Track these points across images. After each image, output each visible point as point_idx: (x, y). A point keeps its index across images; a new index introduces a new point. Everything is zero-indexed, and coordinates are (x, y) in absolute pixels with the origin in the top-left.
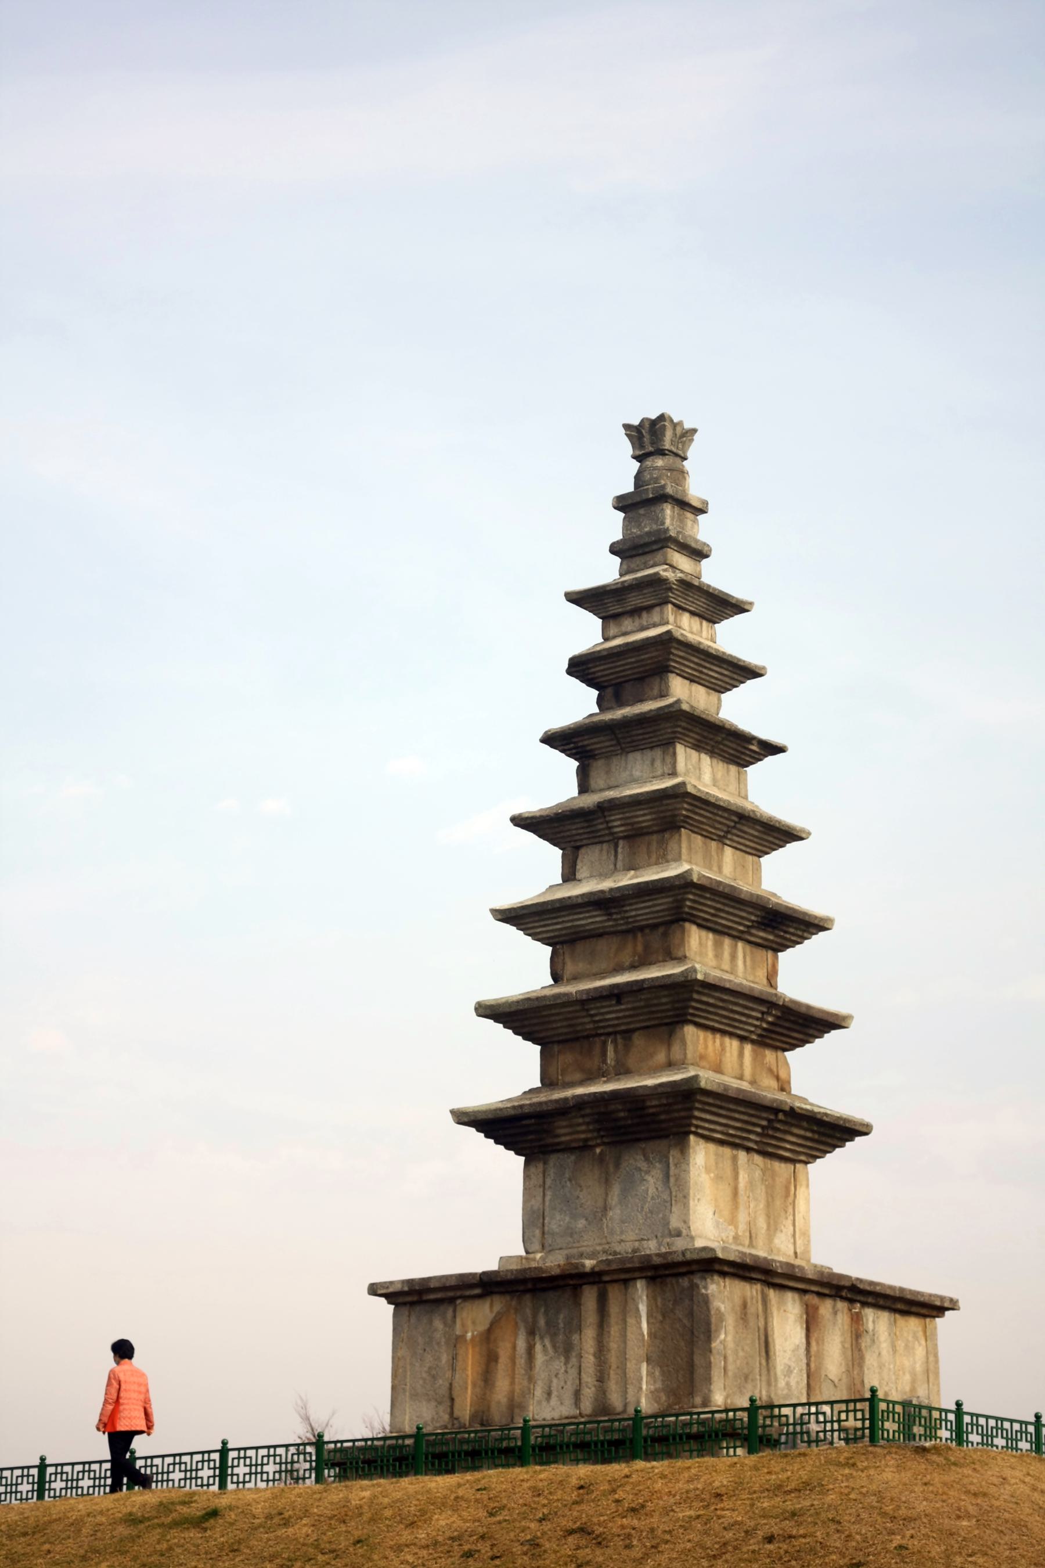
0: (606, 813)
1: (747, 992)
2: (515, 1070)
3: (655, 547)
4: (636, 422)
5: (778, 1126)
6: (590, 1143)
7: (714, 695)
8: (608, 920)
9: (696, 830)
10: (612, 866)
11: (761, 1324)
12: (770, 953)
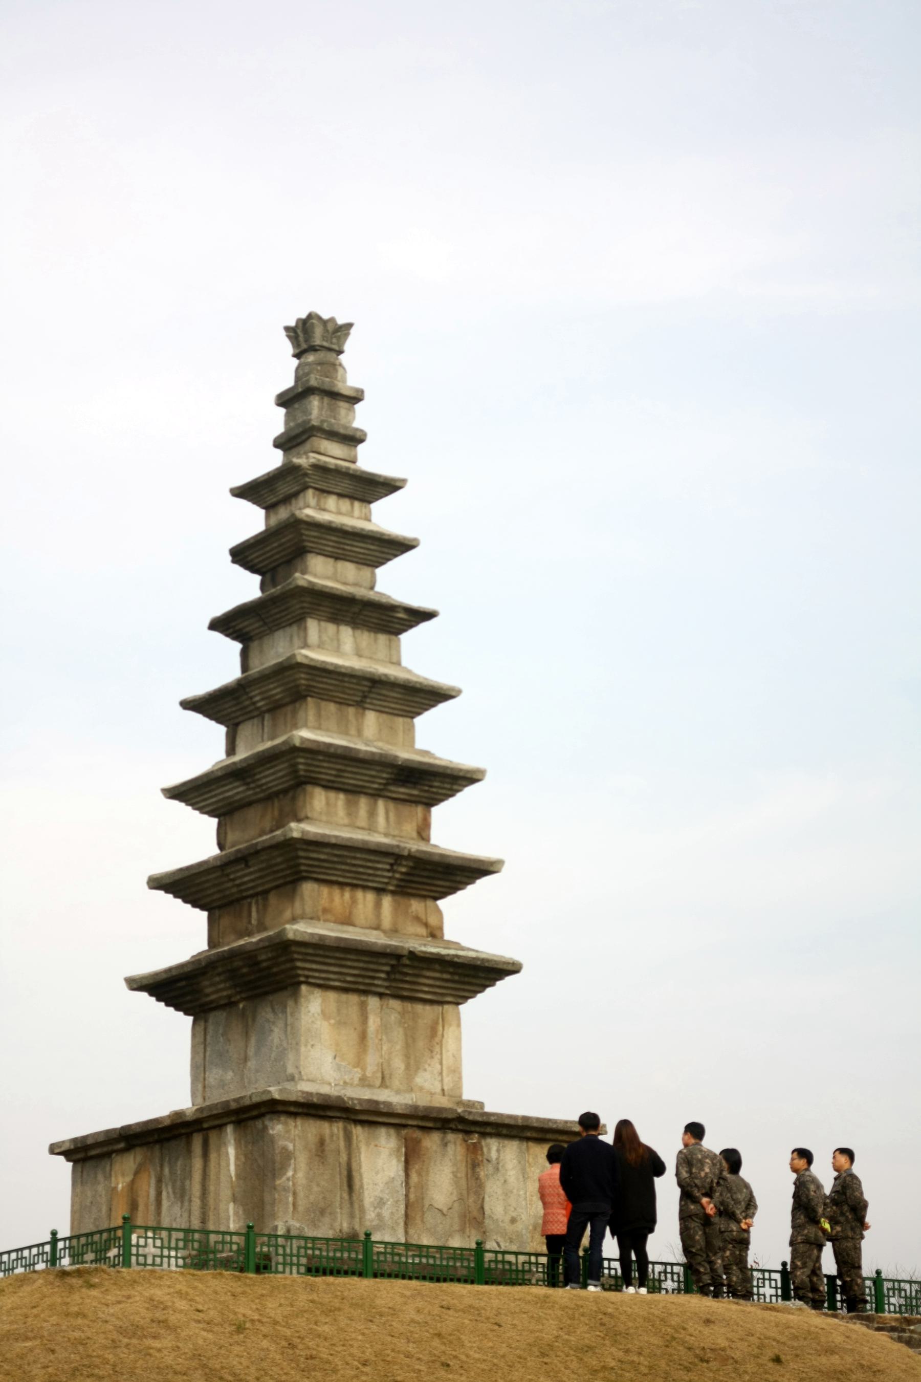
0: (247, 690)
1: (360, 846)
3: (304, 437)
4: (293, 324)
5: (405, 970)
6: (233, 999)
7: (366, 572)
8: (248, 789)
9: (325, 697)
10: (260, 739)
11: (344, 1158)
12: (420, 809)
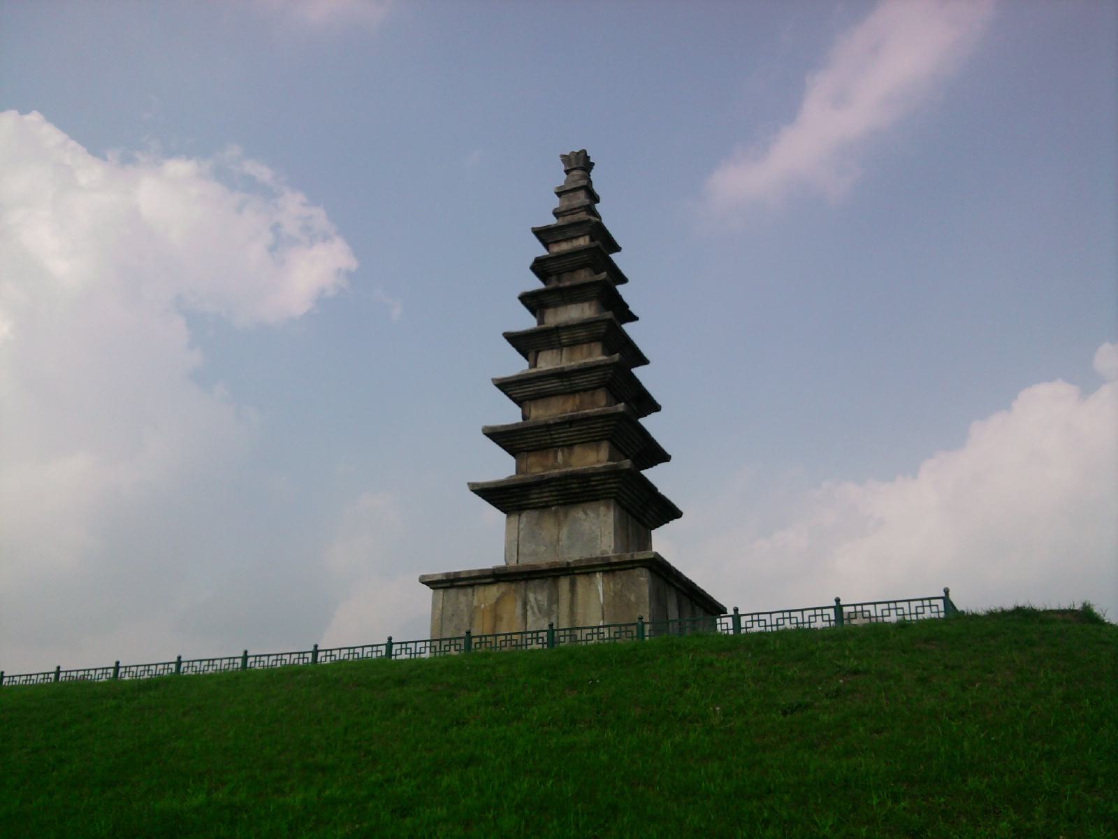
2: (501, 466)
6: (550, 504)
